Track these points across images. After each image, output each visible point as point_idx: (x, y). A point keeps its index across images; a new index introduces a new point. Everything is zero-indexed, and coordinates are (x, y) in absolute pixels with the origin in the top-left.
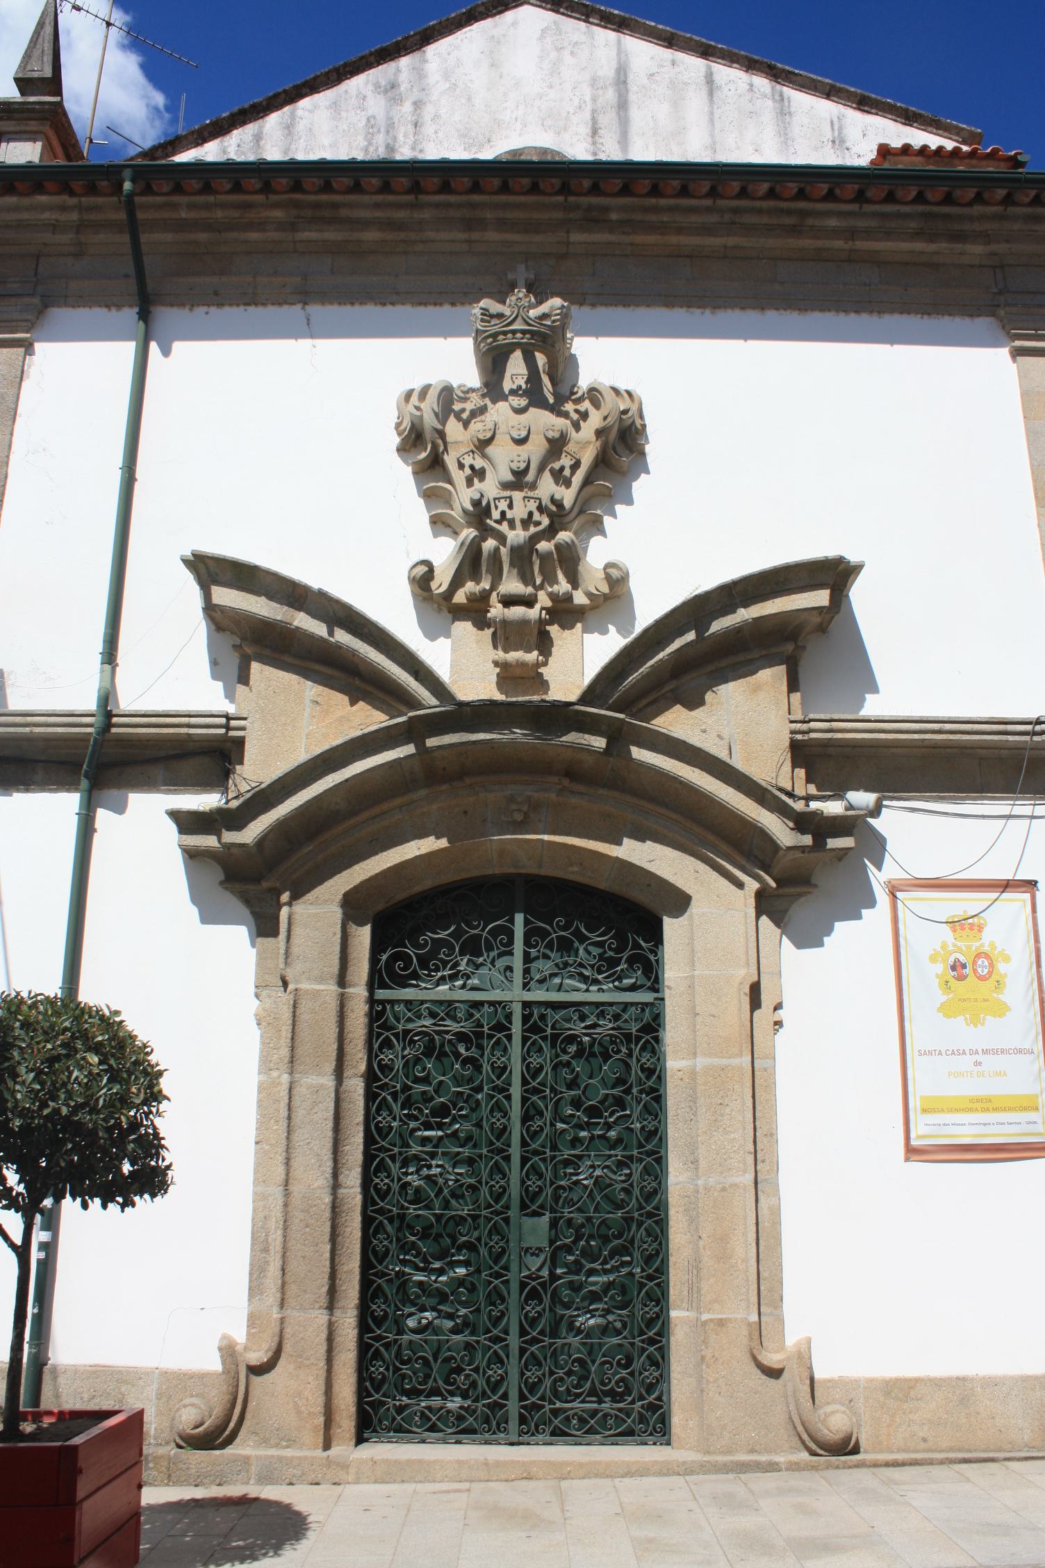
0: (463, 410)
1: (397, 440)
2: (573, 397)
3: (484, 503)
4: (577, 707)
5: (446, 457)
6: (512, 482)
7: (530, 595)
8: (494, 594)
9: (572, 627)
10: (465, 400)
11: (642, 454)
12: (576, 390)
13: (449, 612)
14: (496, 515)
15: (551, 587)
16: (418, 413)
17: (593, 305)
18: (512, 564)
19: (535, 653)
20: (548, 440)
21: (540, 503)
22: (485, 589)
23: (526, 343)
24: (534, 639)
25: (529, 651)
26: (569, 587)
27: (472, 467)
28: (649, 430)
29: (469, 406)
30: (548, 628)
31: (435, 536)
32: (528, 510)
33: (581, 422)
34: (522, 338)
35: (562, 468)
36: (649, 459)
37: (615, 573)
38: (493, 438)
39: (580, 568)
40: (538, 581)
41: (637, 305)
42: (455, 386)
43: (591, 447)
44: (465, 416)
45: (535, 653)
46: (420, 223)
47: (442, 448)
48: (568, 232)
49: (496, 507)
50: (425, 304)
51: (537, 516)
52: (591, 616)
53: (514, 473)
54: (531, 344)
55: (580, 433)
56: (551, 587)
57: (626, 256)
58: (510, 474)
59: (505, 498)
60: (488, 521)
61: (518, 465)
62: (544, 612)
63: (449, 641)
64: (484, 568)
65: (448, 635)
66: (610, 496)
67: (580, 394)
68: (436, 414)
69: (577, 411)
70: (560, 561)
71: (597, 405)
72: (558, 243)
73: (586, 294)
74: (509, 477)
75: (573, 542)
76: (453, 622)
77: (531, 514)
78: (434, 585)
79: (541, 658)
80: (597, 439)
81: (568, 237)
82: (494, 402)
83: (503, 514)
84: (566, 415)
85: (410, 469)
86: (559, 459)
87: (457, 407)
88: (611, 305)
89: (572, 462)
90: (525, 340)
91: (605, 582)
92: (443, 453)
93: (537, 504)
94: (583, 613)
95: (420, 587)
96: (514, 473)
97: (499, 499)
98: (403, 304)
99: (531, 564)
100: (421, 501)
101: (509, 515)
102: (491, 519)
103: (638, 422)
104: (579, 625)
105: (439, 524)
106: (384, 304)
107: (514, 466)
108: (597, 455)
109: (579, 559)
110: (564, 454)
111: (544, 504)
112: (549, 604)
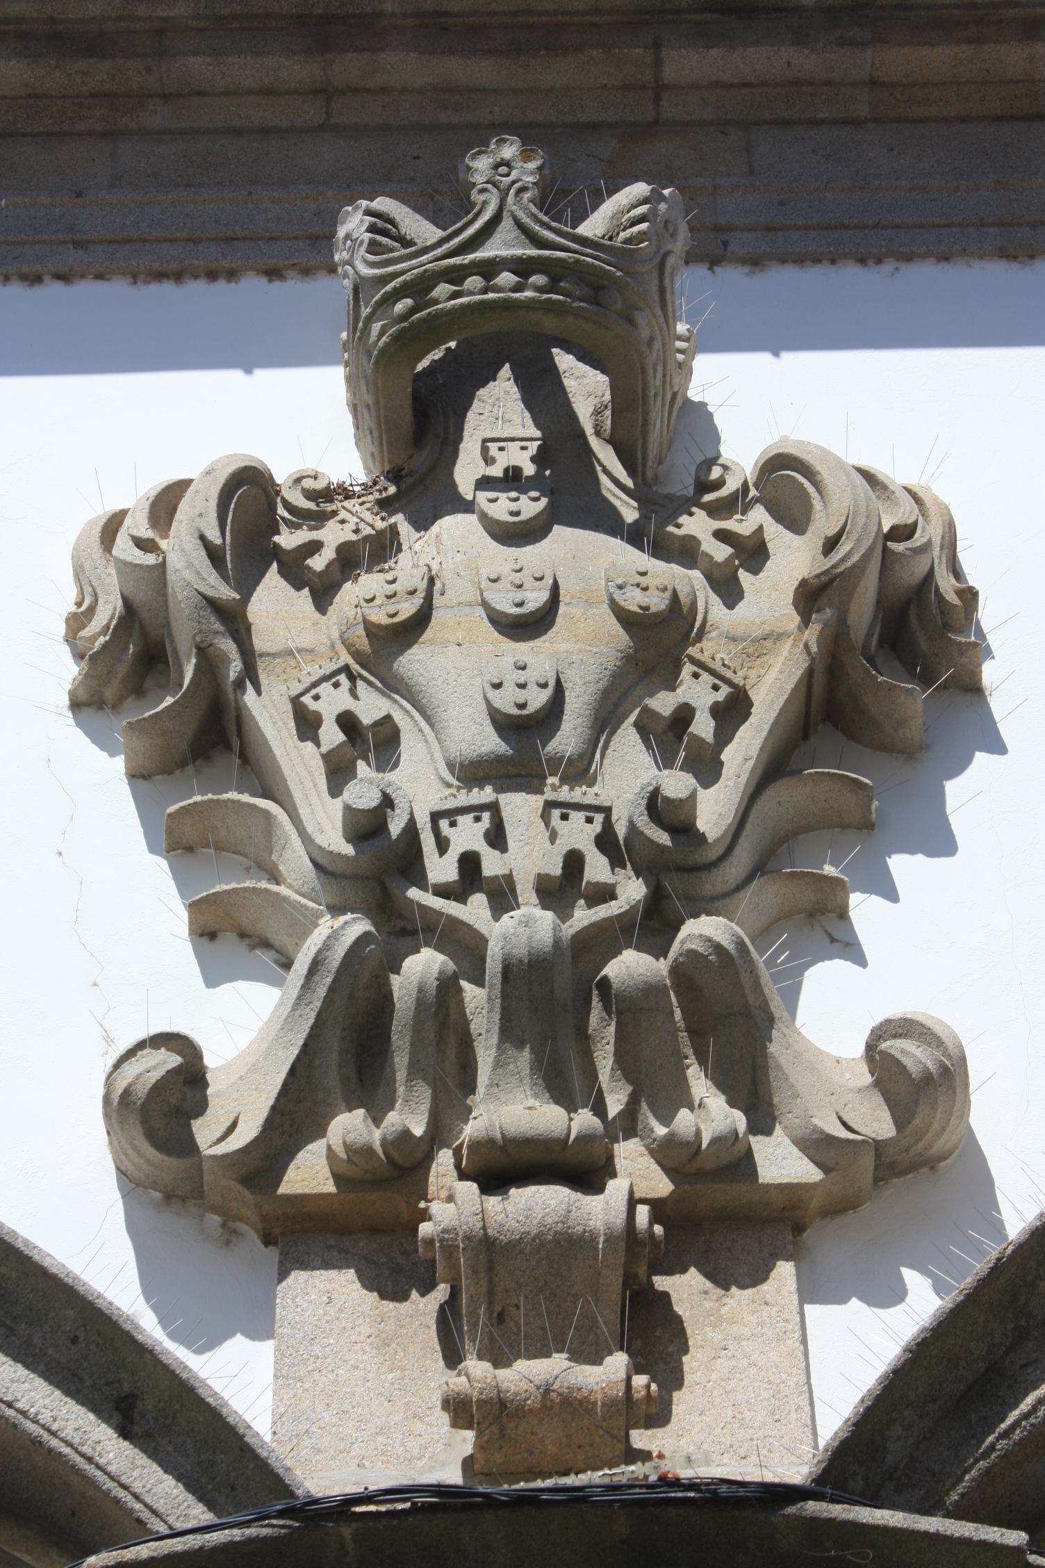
0: (314, 547)
1: (67, 671)
2: (708, 498)
3: (396, 827)
4: (813, 1507)
5: (250, 697)
6: (499, 760)
7: (584, 1139)
8: (445, 1158)
9: (758, 1276)
10: (318, 519)
11: (973, 689)
12: (716, 473)
13: (268, 1240)
14: (442, 869)
15: (666, 1120)
16: (150, 559)
17: (755, 262)
18: (510, 1033)
19: (618, 1362)
20: (626, 618)
21: (608, 825)
22: (406, 1134)
23: (530, 305)
24: (607, 1320)
25: (591, 1354)
26: (739, 1120)
27: (347, 722)
28: (988, 615)
29: (333, 535)
30: (662, 1283)
31: (212, 978)
32: (563, 846)
33: (743, 575)
34: (518, 288)
35: (684, 715)
36: (998, 705)
37: (913, 1054)
38: (421, 619)
39: (773, 1048)
40: (615, 1104)
41: (909, 258)
42: (281, 476)
43: (786, 648)
44: (318, 563)
45: (618, 1362)
46: (160, 32)
47: (235, 668)
48: (657, 45)
49: (442, 845)
50: (178, 277)
51: (597, 868)
52: (820, 1236)
53: (504, 724)
54: (549, 307)
55: (741, 607)
56: (666, 1120)
57: (857, 123)
58: (490, 730)
59: (475, 810)
60: (414, 893)
61: (521, 696)
62: (643, 1213)
63: (269, 1345)
64: (401, 1061)
65: (261, 1327)
66: (867, 826)
67: (732, 485)
68: (214, 555)
69: (723, 536)
70: (695, 1034)
71: (795, 519)
72: (625, 87)
73: (730, 228)
74: (490, 742)
75: (741, 945)
76: (283, 1275)
77: (574, 861)
78: (205, 1132)
79: (640, 1381)
80: (806, 621)
81: (658, 64)
82: (422, 523)
83: (469, 862)
84: (686, 552)
85: (118, 765)
86: (671, 684)
87: (288, 539)
88: (817, 261)
89: (721, 696)
90: (528, 294)
91: (878, 1099)
92: (239, 685)
93: (597, 827)
94: (799, 1229)
95: (151, 1136)
96: (504, 724)
97: (452, 815)
98: (100, 277)
99: (584, 1041)
100: (160, 866)
101: (492, 864)
102: (422, 884)
103: (946, 584)
104: (785, 1271)
105: (228, 940)
106: (35, 279)
107: (505, 701)
108: (810, 674)
109: (771, 1020)
110: (688, 669)
111: (621, 830)
112: (662, 1186)
